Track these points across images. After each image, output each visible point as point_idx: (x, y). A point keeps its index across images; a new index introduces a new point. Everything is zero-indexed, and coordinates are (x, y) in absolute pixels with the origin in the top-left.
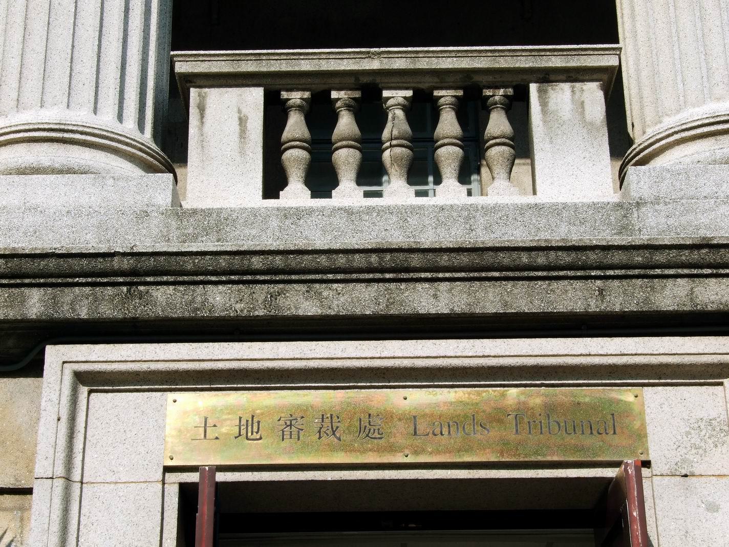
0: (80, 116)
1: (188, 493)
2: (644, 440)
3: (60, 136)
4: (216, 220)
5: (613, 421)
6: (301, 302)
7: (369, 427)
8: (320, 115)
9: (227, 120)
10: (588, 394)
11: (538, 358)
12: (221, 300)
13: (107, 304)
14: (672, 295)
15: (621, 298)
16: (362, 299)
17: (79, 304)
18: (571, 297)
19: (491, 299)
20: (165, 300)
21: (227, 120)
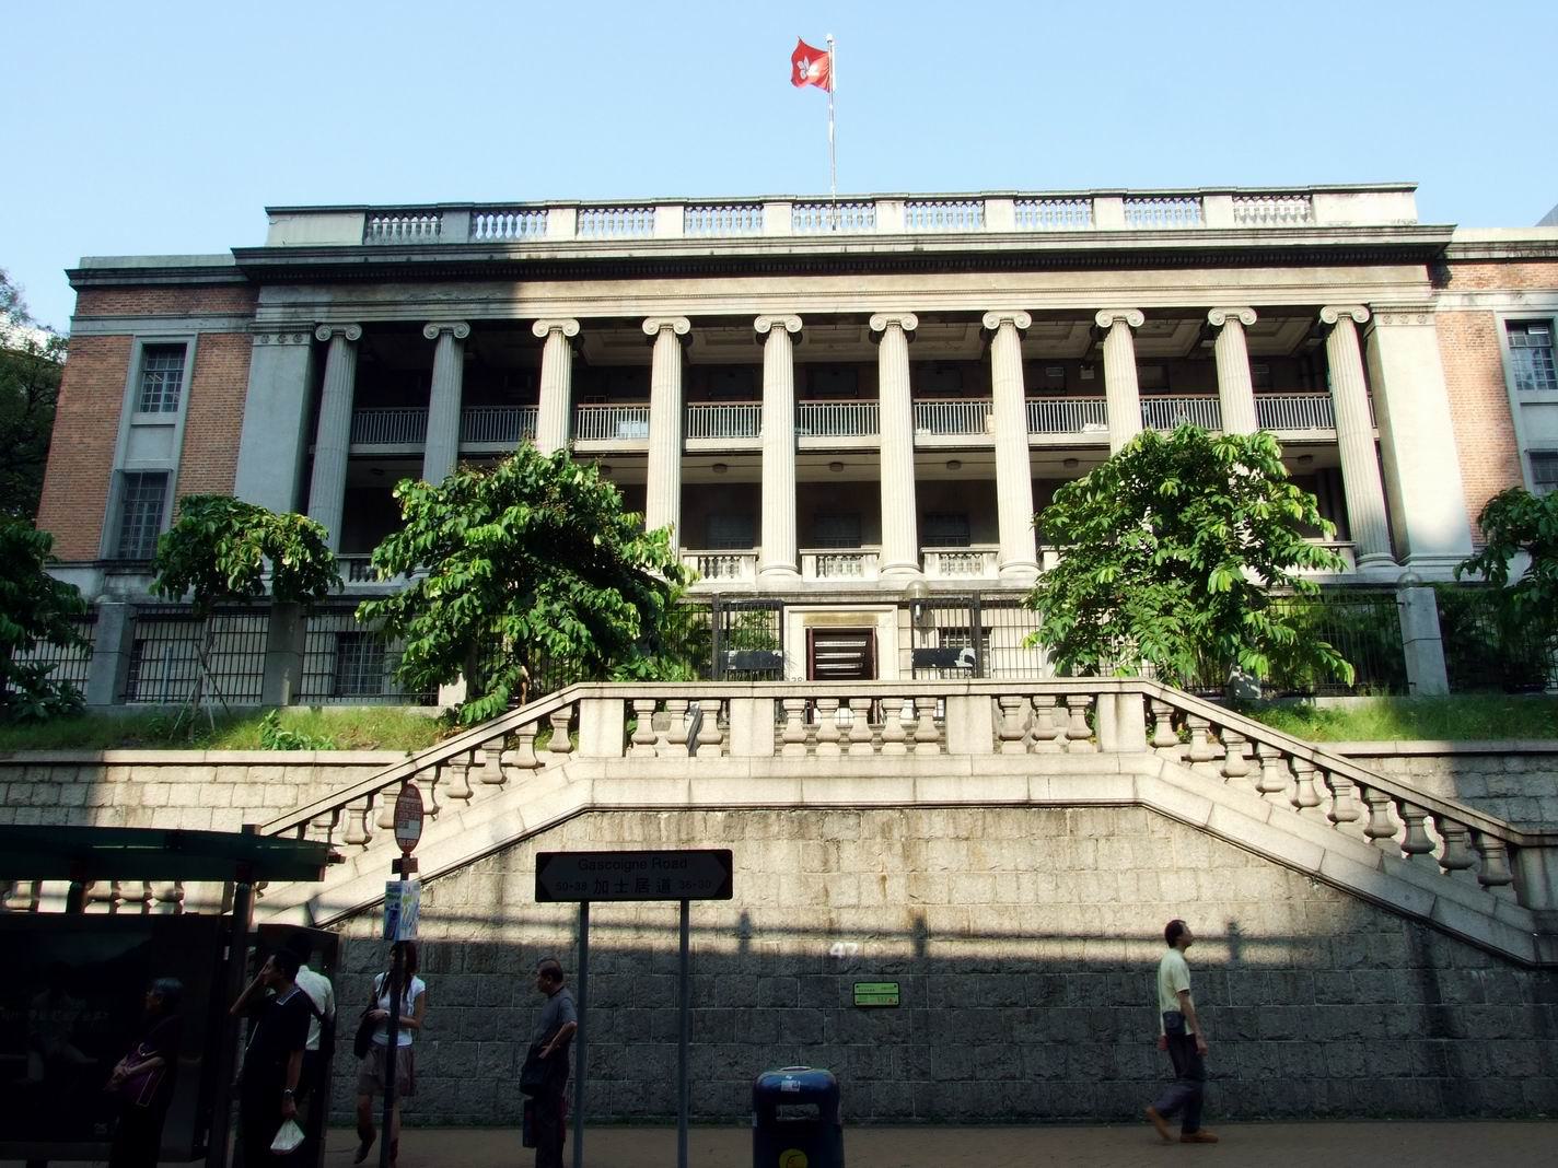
0: (784, 564)
1: (807, 631)
2: (1175, 1131)
3: (781, 567)
4: (809, 585)
5: (872, 618)
6: (824, 600)
7: (835, 619)
8: (707, 561)
9: (809, 562)
10: (870, 614)
11: (953, 798)
12: (811, 599)
13: (794, 600)
14: (883, 599)
15: (875, 599)
16: (834, 599)
17: (789, 600)
18: (867, 599)
19: (854, 599)
20: (803, 599)
21: (809, 562)
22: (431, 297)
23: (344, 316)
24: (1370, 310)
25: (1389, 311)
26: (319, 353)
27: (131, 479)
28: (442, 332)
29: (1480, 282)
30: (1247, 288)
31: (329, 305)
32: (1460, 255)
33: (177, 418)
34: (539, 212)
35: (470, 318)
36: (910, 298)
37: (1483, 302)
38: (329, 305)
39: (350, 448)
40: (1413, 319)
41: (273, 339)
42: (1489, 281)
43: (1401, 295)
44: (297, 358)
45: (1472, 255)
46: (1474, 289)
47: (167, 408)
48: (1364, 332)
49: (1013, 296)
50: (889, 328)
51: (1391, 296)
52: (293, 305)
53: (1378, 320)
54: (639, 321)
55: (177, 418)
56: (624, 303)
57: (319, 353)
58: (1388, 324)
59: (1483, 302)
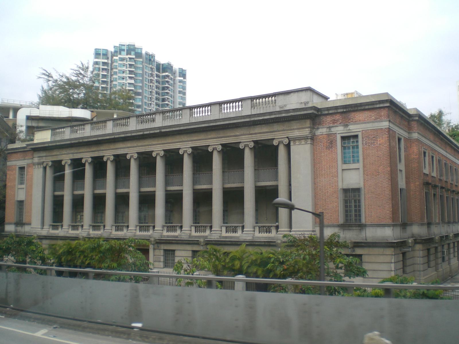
22: (63, 153)
23: (49, 159)
24: (289, 139)
25: (296, 139)
26: (45, 168)
27: (346, 191)
28: (214, 149)
29: (334, 122)
30: (252, 134)
31: (45, 156)
32: (326, 112)
33: (360, 165)
34: (119, 120)
35: (164, 149)
36: (162, 145)
37: (334, 130)
38: (45, 156)
39: (255, 184)
40: (303, 142)
41: (37, 166)
42: (337, 121)
43: (300, 132)
44: (41, 170)
45: (331, 112)
46: (331, 125)
47: (354, 162)
48: (288, 147)
49: (187, 143)
50: (185, 153)
51: (297, 133)
52: (39, 157)
53: (292, 143)
54: (81, 159)
55: (360, 165)
56: (100, 152)
57: (45, 168)
58: (295, 144)
59: (334, 130)
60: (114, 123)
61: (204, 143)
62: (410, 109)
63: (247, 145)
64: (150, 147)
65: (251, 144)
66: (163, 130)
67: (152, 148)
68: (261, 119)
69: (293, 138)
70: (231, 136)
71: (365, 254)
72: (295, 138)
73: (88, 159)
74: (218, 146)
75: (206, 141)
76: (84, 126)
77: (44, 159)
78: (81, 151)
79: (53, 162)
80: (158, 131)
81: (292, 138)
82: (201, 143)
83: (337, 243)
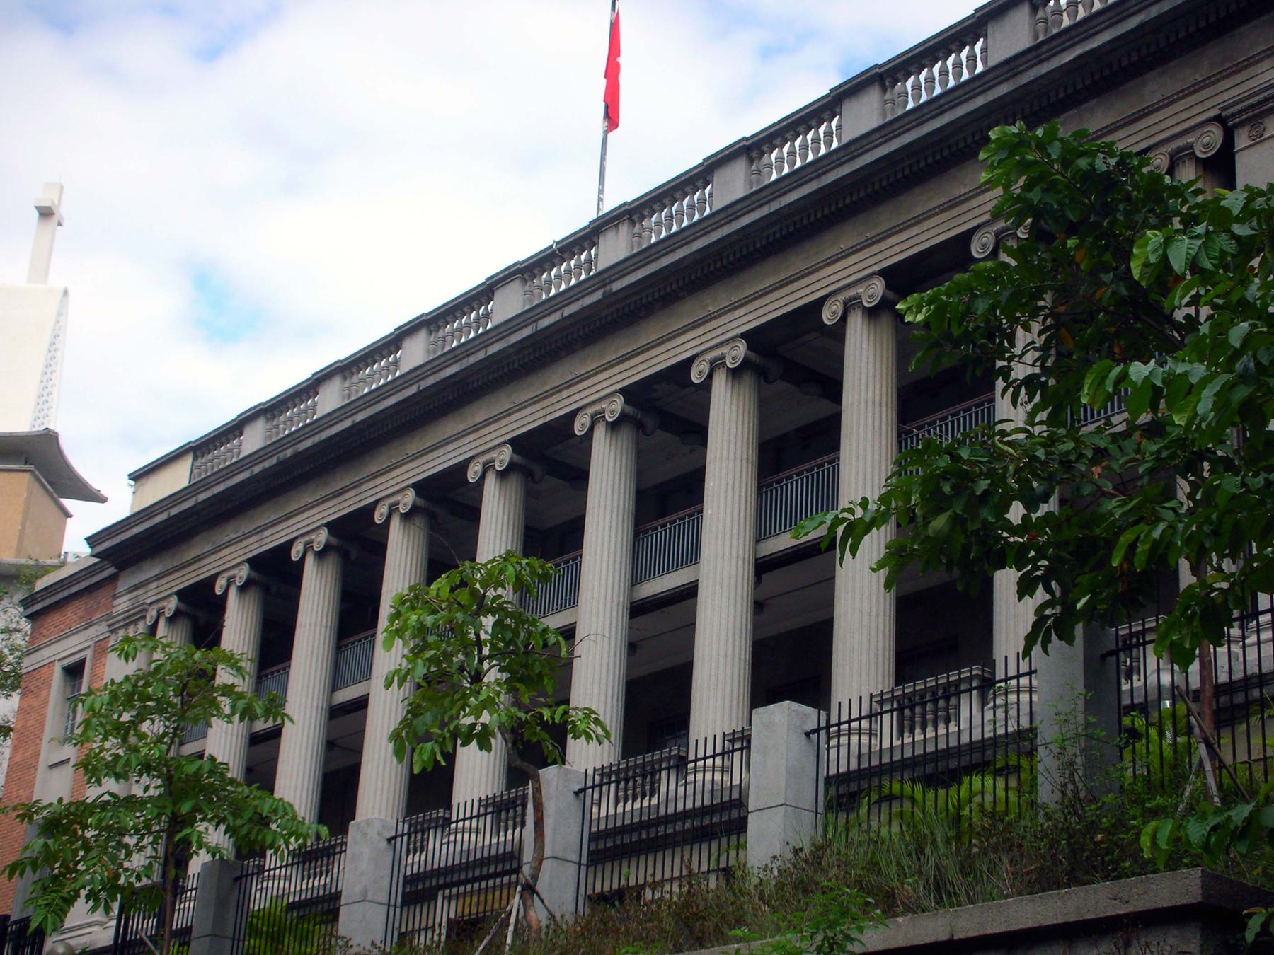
28: (848, 307)
35: (250, 555)
38: (159, 577)
50: (596, 428)
54: (370, 509)
58: (1258, 140)
60: (754, 167)
61: (496, 434)
62: (132, 508)
63: (1180, 150)
64: (565, 394)
65: (1207, 140)
66: (617, 286)
67: (576, 397)
68: (1070, 58)
69: (1247, 109)
70: (927, 216)
71: (543, 896)
72: (1260, 103)
73: (1190, 139)
74: (865, 285)
75: (882, 246)
76: (594, 244)
77: (150, 594)
78: (294, 506)
79: (182, 594)
80: (597, 296)
81: (1240, 112)
82: (670, 354)
83: (515, 865)
